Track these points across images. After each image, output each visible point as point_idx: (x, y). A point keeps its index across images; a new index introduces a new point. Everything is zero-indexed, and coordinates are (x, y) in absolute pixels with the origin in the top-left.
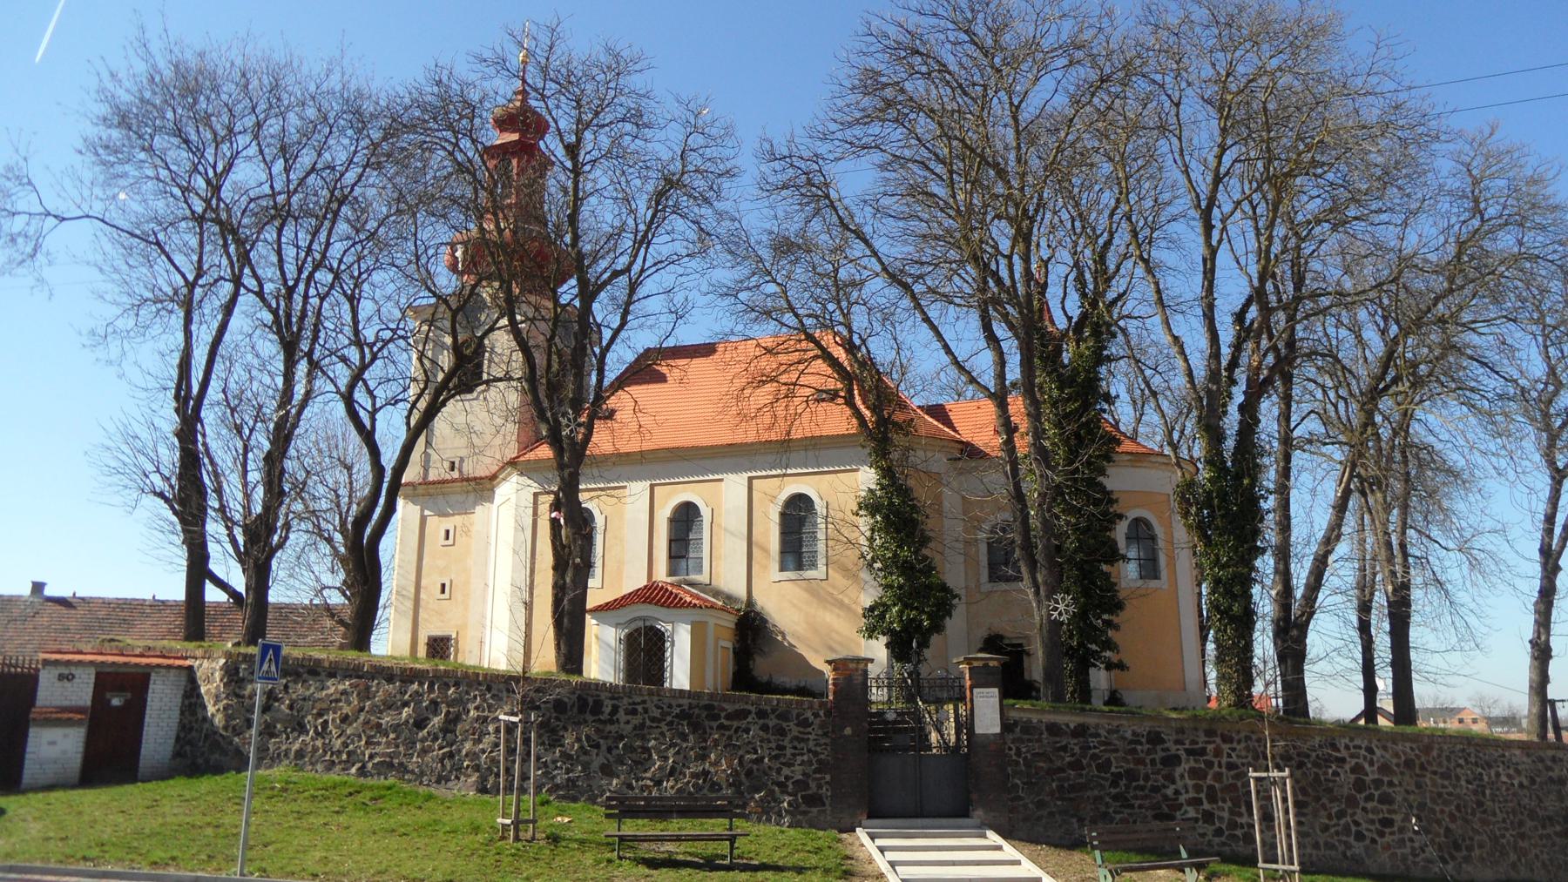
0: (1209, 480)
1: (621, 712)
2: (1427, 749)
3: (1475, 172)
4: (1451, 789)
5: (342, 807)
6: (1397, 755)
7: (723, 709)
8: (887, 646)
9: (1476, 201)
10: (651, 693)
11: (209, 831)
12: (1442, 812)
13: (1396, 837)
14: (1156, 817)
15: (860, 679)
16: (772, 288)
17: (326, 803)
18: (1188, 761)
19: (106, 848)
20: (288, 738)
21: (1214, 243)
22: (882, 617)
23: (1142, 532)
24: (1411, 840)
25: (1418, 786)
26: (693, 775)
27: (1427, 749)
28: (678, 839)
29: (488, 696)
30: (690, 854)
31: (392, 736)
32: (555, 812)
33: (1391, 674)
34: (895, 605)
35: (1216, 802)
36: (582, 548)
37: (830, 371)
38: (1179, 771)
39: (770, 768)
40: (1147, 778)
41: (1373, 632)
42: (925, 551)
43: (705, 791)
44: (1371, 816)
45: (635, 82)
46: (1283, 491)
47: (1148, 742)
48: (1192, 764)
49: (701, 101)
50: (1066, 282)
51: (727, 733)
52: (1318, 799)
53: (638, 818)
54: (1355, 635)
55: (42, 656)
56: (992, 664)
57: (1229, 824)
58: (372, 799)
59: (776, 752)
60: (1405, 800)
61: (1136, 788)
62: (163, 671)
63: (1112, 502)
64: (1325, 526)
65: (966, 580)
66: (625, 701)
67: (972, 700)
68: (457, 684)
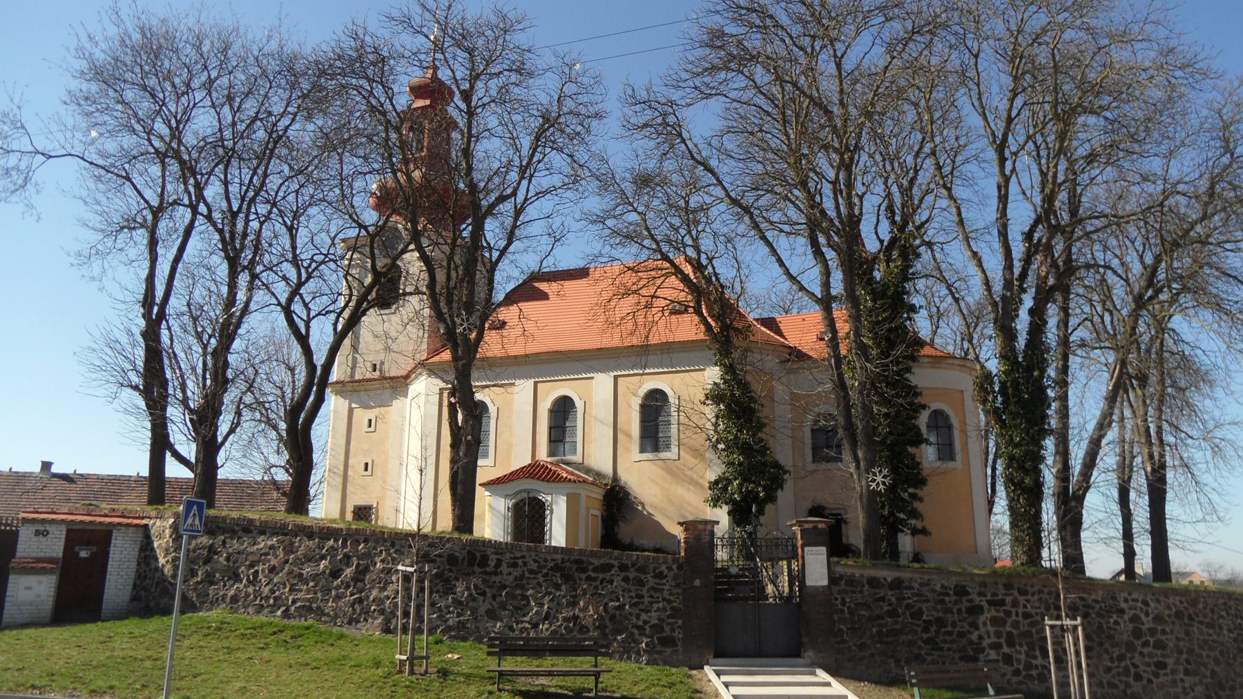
0: (1004, 372)
1: (504, 565)
2: (1194, 603)
3: (1225, 118)
4: (1215, 637)
5: (266, 644)
6: (1169, 607)
7: (591, 564)
8: (729, 513)
9: (1226, 141)
10: (529, 549)
11: (148, 664)
12: (1208, 656)
13: (1170, 678)
14: (962, 659)
15: (708, 538)
16: (633, 217)
17: (254, 641)
18: (990, 610)
19: (55, 678)
20: (225, 586)
21: (1007, 172)
22: (725, 489)
23: (940, 421)
24: (1182, 681)
25: (1187, 633)
26: (565, 619)
27: (1194, 603)
28: (550, 674)
29: (392, 551)
30: (561, 687)
31: (311, 584)
32: (446, 650)
33: (1150, 542)
34: (736, 479)
35: (1014, 646)
36: (473, 427)
37: (681, 286)
38: (982, 619)
39: (630, 614)
40: (954, 624)
41: (1132, 507)
42: (760, 435)
43: (575, 633)
44: (1147, 659)
45: (519, 39)
46: (1063, 384)
47: (955, 594)
48: (993, 613)
49: (575, 56)
50: (879, 210)
51: (594, 583)
52: (1101, 644)
53: (516, 655)
54: (1116, 508)
55: (22, 515)
56: (820, 526)
57: (1025, 665)
58: (292, 637)
59: (636, 600)
60: (1176, 645)
61: (945, 633)
62: (123, 528)
63: (916, 394)
64: (1098, 413)
65: (794, 459)
66: (508, 555)
67: (803, 557)
68: (366, 541)
